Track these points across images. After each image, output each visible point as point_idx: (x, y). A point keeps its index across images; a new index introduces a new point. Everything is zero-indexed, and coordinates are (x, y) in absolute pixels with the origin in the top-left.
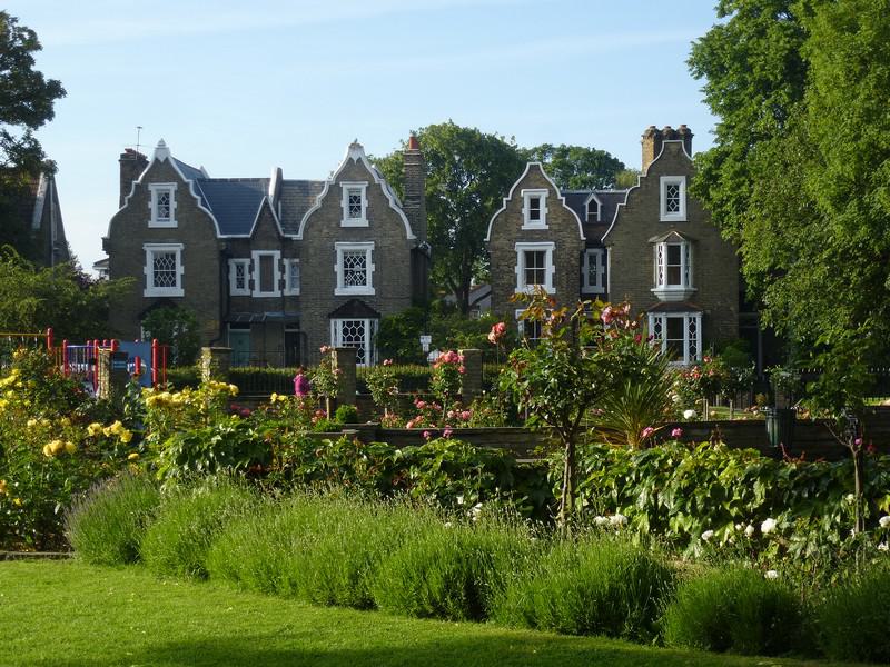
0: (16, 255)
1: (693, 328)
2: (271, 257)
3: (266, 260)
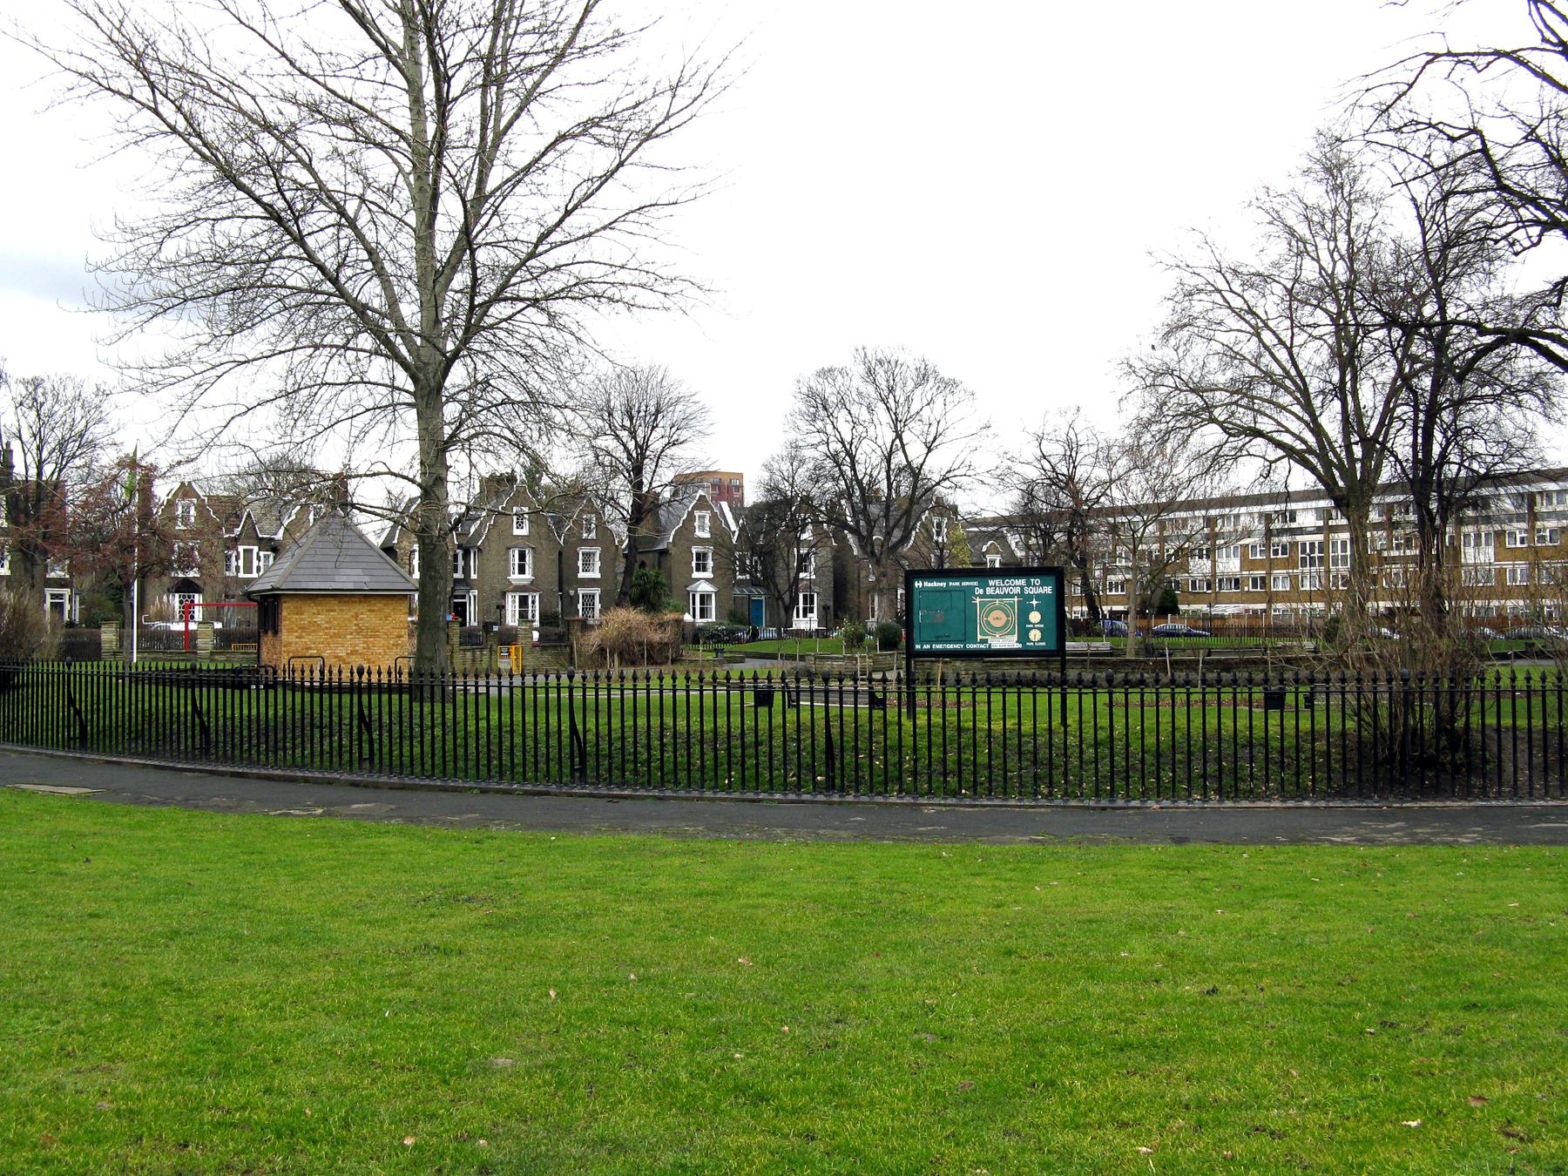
0: (1348, 553)
1: (533, 602)
2: (251, 551)
3: (248, 552)
